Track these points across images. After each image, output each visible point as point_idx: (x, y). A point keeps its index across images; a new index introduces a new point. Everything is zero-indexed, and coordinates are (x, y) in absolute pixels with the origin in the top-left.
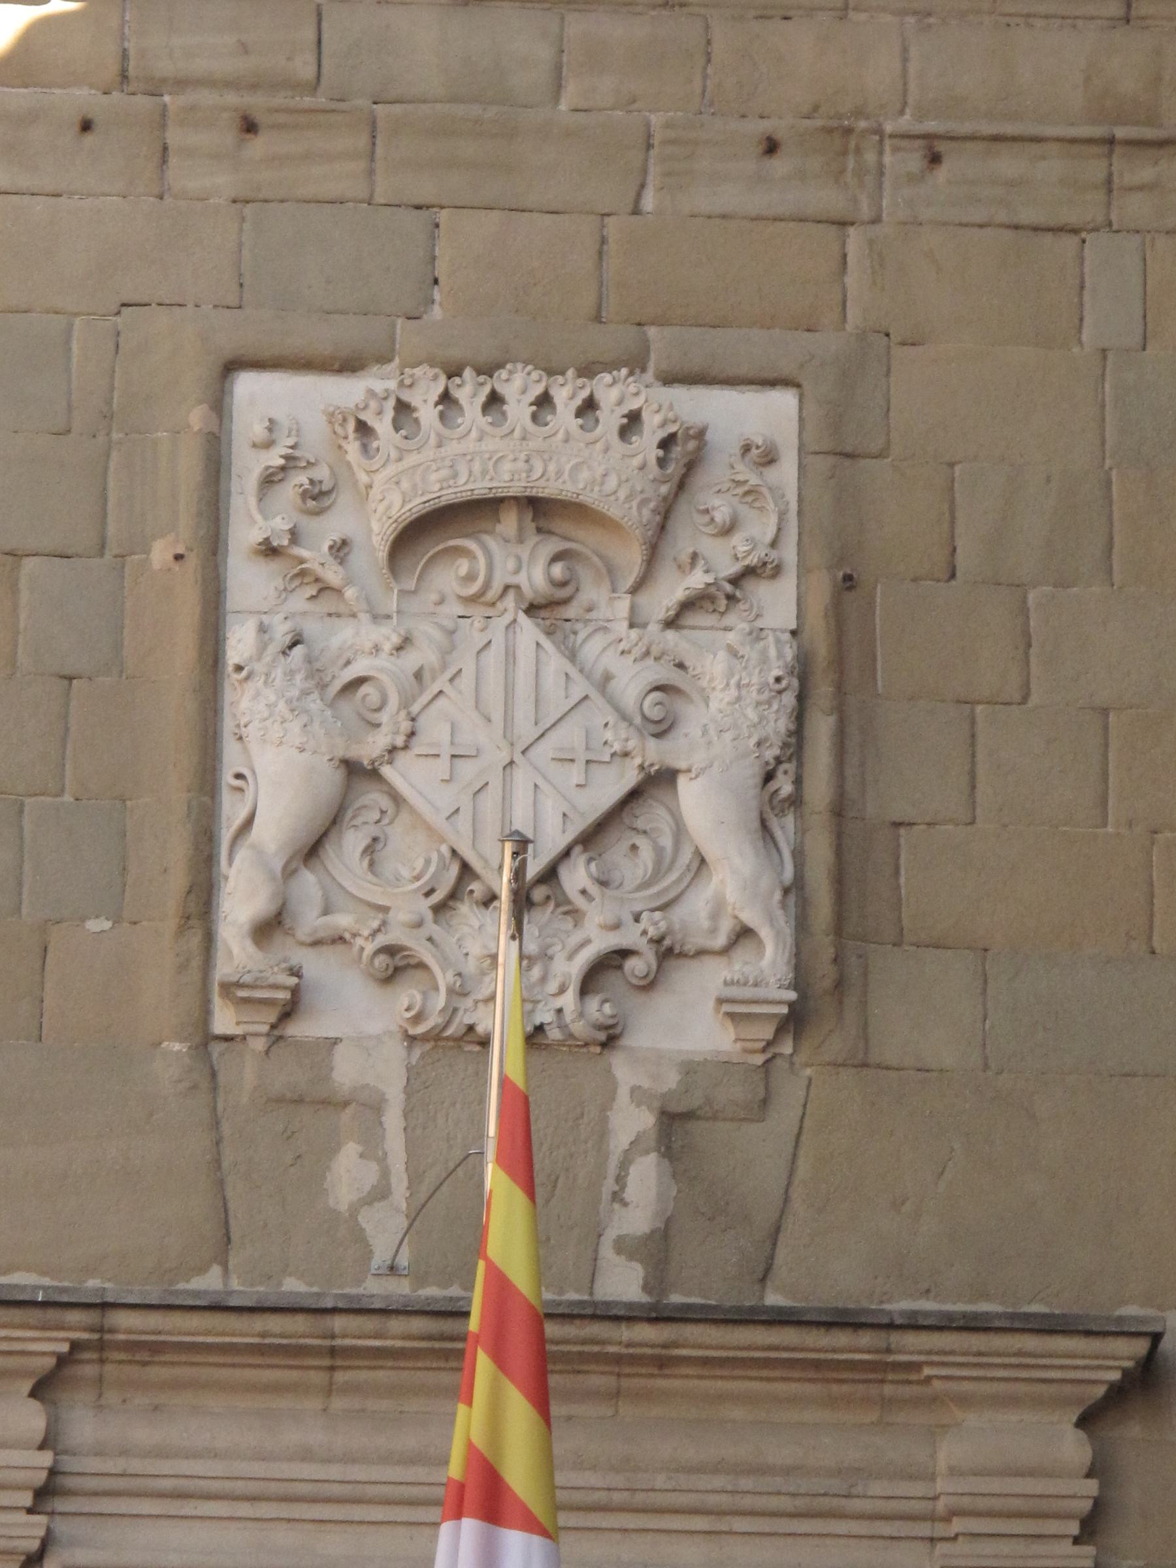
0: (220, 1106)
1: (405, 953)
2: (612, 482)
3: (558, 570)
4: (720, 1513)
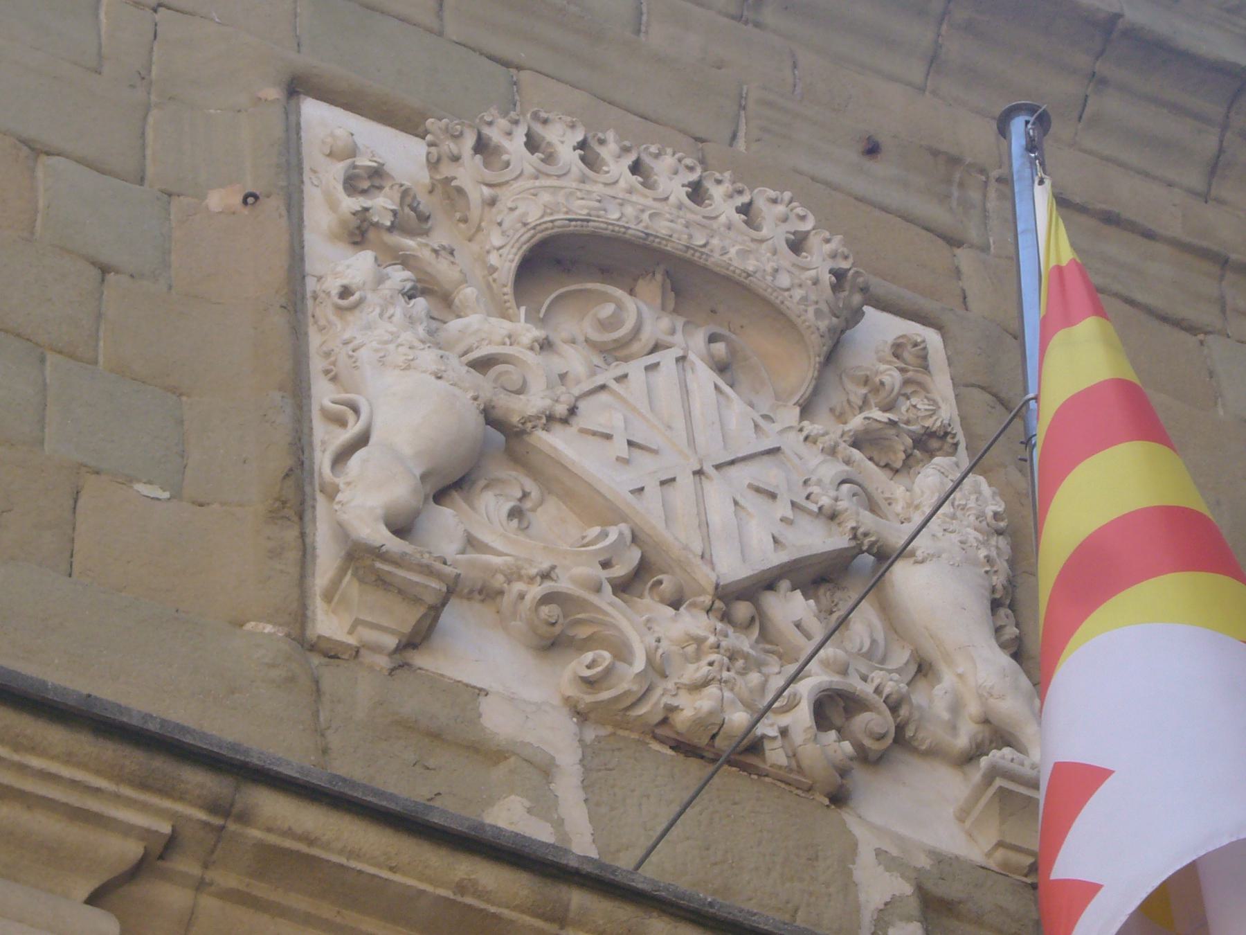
0: (323, 716)
1: (580, 616)
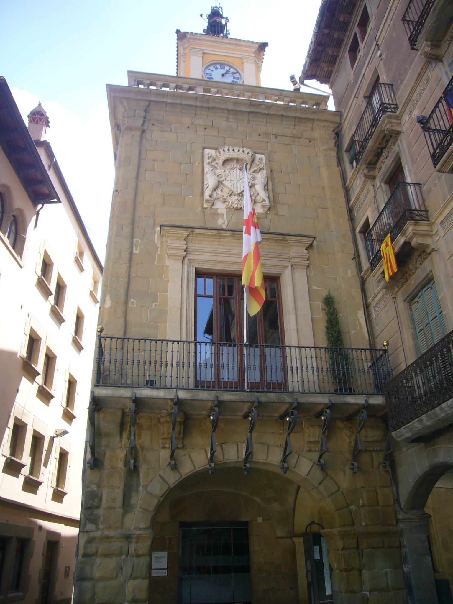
2: (247, 158)
3: (241, 166)
4: (265, 257)
